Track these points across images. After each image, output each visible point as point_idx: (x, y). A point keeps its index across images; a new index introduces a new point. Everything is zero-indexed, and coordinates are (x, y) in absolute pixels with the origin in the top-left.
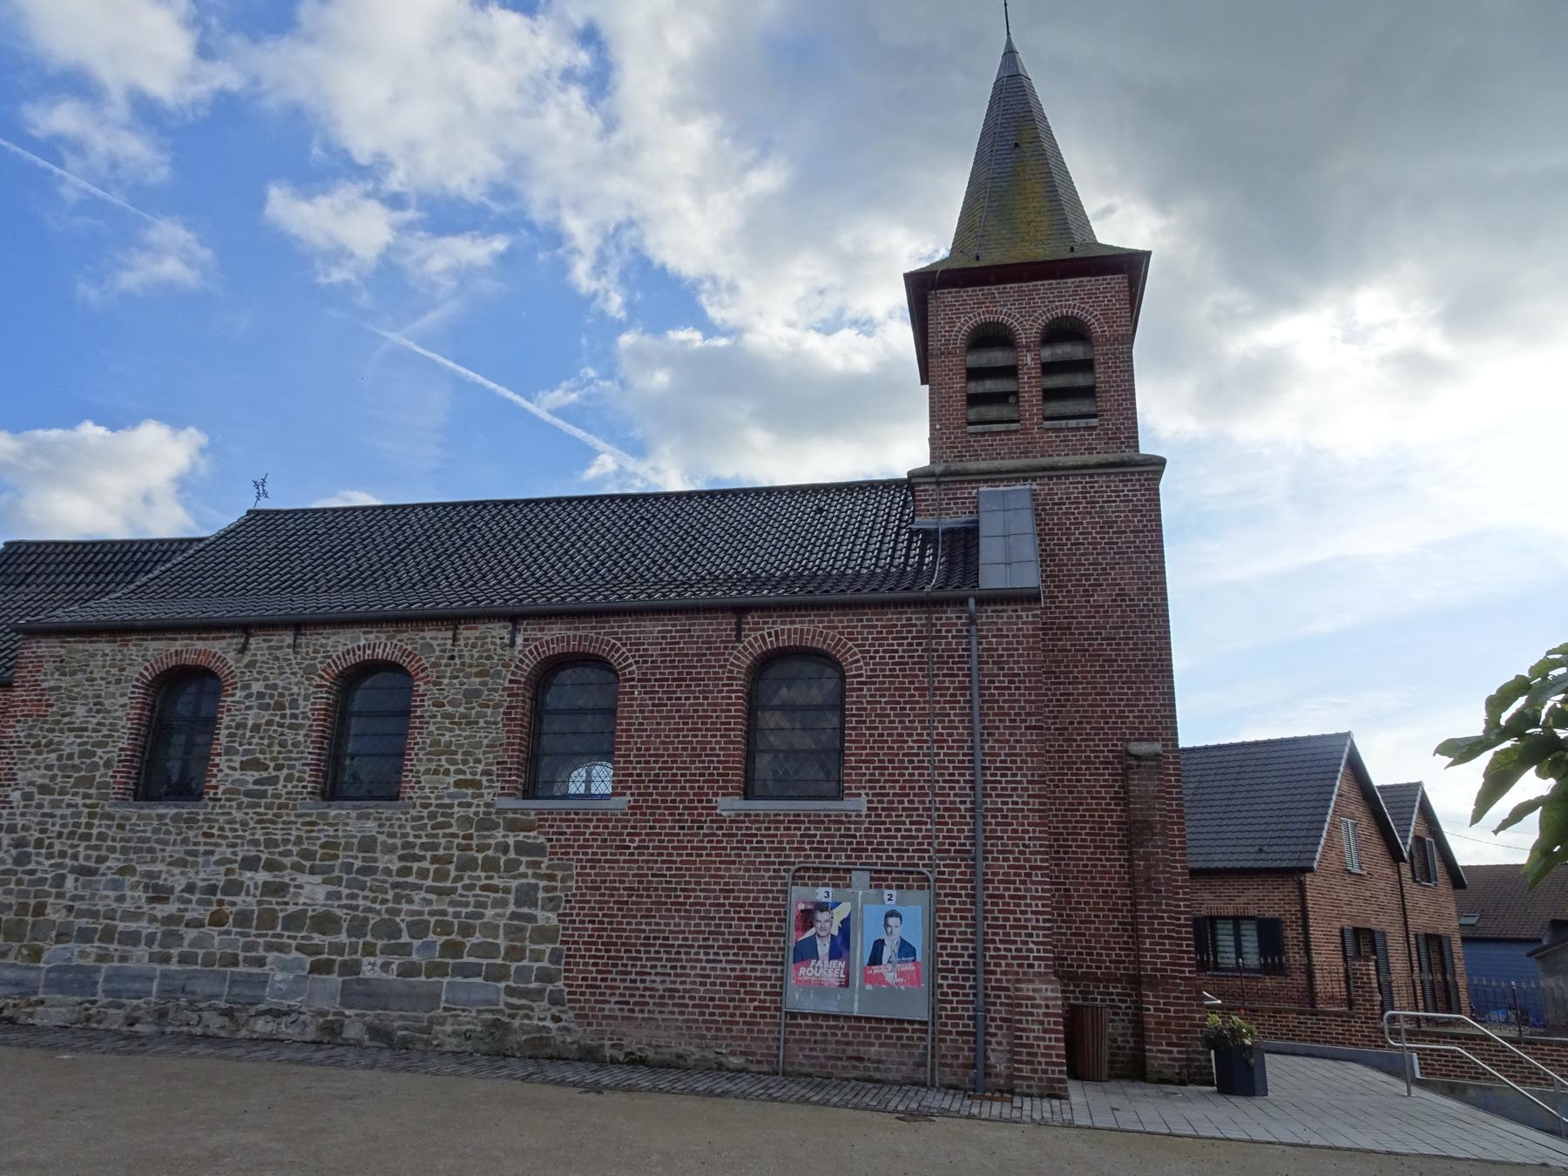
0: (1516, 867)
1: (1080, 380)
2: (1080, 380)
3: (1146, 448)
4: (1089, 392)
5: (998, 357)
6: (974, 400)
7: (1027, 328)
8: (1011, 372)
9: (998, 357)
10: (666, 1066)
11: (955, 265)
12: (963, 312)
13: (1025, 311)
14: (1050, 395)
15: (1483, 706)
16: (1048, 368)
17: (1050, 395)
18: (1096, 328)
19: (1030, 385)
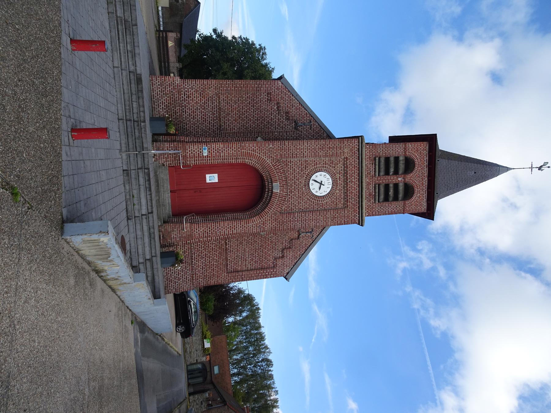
0: (206, 180)
1: (392, 170)
2: (392, 170)
3: (368, 220)
4: (386, 199)
5: (402, 166)
6: (387, 159)
7: (411, 178)
8: (396, 173)
9: (402, 166)
10: (131, 259)
11: (437, 150)
12: (419, 153)
13: (418, 178)
14: (387, 187)
15: (252, 38)
16: (396, 186)
17: (387, 187)
18: (407, 202)
19: (392, 179)
